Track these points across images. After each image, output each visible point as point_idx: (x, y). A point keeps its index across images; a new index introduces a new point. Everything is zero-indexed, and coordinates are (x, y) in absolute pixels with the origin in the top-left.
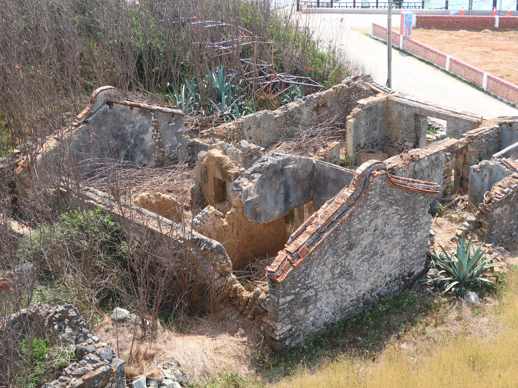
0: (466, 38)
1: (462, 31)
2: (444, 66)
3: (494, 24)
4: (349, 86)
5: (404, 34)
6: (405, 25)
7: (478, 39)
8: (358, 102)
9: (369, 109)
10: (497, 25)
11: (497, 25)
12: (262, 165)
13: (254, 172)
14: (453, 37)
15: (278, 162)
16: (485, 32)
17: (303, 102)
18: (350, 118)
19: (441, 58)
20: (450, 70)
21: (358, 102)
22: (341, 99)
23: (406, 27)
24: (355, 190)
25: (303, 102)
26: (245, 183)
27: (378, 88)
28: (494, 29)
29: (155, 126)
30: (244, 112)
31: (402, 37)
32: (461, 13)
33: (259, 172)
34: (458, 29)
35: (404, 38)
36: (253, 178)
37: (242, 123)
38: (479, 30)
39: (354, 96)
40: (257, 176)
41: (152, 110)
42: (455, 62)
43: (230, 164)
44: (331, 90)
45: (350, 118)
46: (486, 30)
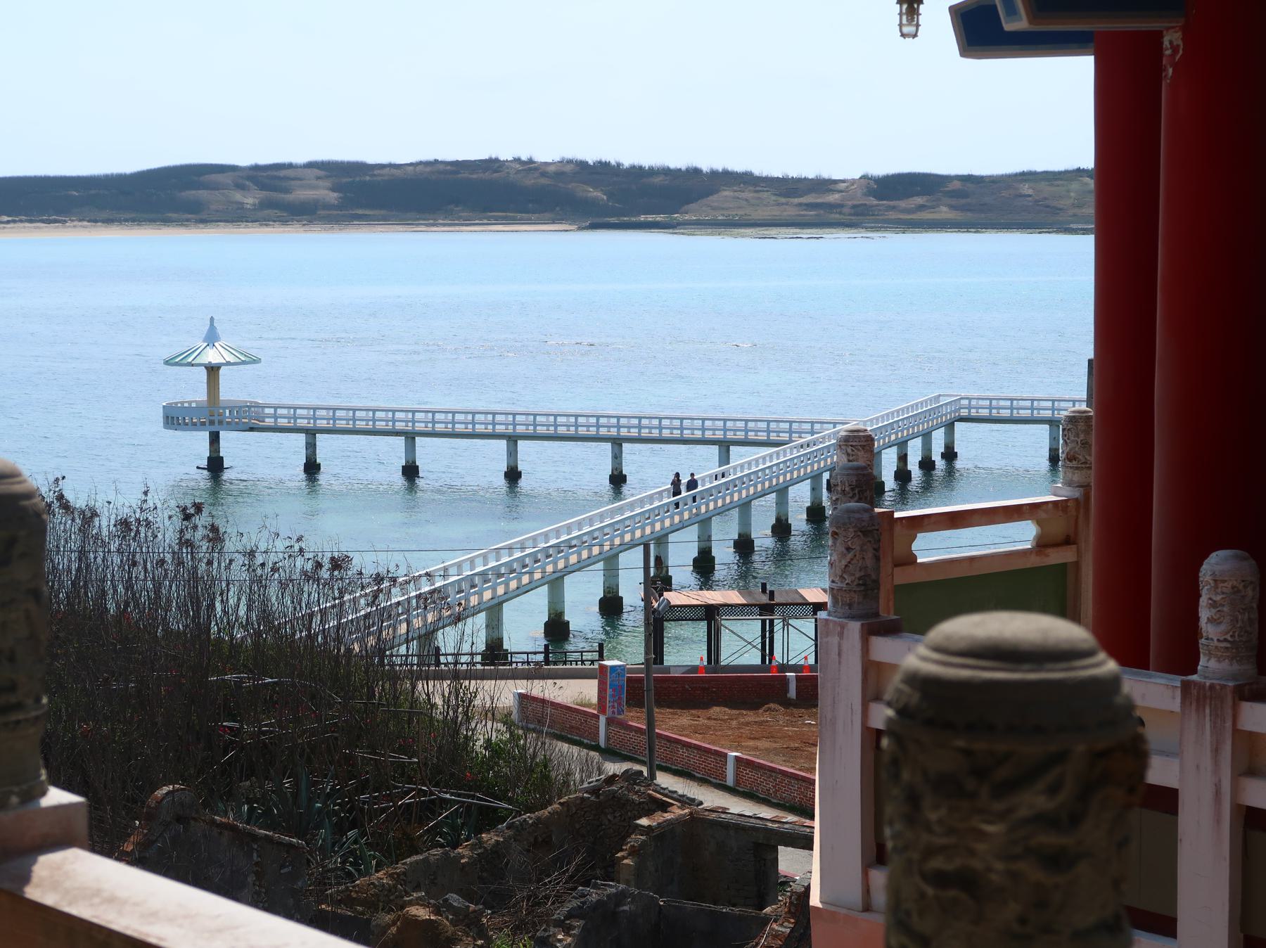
0: (734, 723)
1: (716, 710)
2: (723, 776)
3: (787, 691)
4: (598, 797)
5: (609, 711)
6: (609, 691)
7: (761, 723)
8: (639, 822)
9: (660, 835)
10: (792, 693)
11: (792, 693)
12: (584, 903)
13: (570, 915)
14: (703, 721)
15: (608, 896)
16: (769, 709)
17: (510, 833)
18: (624, 858)
19: (712, 759)
20: (737, 782)
21: (639, 822)
22: (577, 826)
23: (614, 696)
24: (795, 924)
25: (510, 833)
26: (560, 937)
27: (666, 796)
28: (787, 703)
29: (256, 873)
30: (374, 862)
31: (603, 719)
32: (694, 669)
33: (579, 917)
34: (706, 706)
35: (610, 722)
36: (571, 928)
37: (404, 874)
38: (754, 706)
39: (609, 817)
40: (578, 923)
41: (255, 838)
42: (749, 763)
43: (454, 933)
44: (556, 806)
45: (624, 858)
46: (772, 705)
